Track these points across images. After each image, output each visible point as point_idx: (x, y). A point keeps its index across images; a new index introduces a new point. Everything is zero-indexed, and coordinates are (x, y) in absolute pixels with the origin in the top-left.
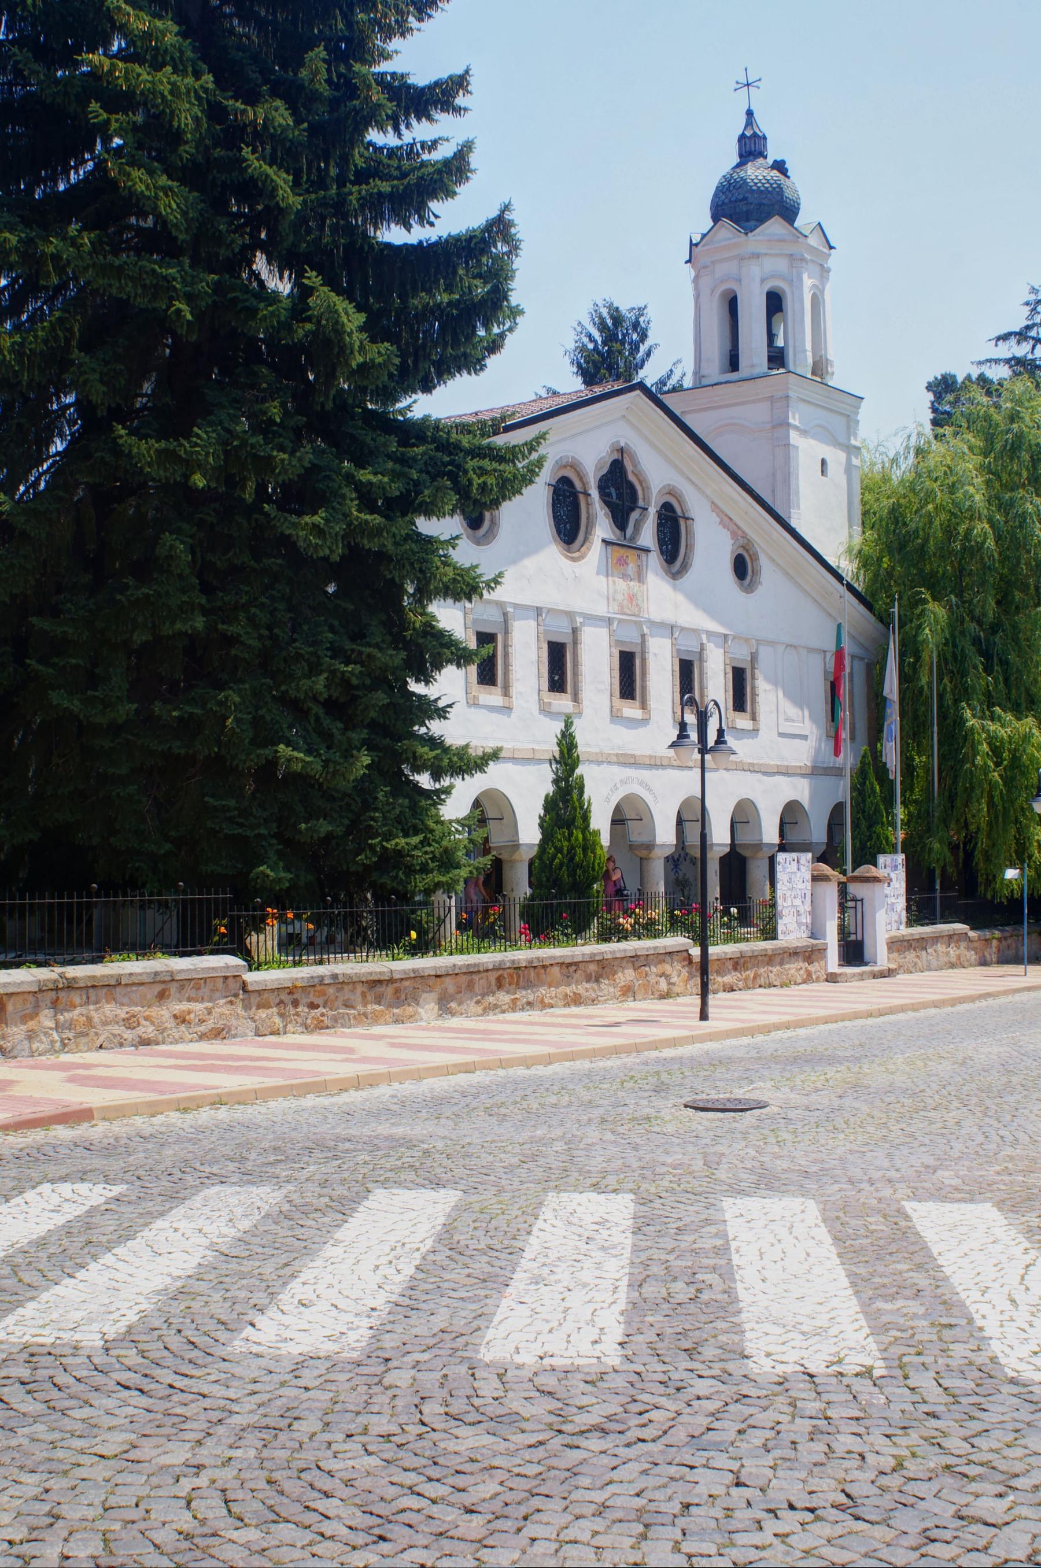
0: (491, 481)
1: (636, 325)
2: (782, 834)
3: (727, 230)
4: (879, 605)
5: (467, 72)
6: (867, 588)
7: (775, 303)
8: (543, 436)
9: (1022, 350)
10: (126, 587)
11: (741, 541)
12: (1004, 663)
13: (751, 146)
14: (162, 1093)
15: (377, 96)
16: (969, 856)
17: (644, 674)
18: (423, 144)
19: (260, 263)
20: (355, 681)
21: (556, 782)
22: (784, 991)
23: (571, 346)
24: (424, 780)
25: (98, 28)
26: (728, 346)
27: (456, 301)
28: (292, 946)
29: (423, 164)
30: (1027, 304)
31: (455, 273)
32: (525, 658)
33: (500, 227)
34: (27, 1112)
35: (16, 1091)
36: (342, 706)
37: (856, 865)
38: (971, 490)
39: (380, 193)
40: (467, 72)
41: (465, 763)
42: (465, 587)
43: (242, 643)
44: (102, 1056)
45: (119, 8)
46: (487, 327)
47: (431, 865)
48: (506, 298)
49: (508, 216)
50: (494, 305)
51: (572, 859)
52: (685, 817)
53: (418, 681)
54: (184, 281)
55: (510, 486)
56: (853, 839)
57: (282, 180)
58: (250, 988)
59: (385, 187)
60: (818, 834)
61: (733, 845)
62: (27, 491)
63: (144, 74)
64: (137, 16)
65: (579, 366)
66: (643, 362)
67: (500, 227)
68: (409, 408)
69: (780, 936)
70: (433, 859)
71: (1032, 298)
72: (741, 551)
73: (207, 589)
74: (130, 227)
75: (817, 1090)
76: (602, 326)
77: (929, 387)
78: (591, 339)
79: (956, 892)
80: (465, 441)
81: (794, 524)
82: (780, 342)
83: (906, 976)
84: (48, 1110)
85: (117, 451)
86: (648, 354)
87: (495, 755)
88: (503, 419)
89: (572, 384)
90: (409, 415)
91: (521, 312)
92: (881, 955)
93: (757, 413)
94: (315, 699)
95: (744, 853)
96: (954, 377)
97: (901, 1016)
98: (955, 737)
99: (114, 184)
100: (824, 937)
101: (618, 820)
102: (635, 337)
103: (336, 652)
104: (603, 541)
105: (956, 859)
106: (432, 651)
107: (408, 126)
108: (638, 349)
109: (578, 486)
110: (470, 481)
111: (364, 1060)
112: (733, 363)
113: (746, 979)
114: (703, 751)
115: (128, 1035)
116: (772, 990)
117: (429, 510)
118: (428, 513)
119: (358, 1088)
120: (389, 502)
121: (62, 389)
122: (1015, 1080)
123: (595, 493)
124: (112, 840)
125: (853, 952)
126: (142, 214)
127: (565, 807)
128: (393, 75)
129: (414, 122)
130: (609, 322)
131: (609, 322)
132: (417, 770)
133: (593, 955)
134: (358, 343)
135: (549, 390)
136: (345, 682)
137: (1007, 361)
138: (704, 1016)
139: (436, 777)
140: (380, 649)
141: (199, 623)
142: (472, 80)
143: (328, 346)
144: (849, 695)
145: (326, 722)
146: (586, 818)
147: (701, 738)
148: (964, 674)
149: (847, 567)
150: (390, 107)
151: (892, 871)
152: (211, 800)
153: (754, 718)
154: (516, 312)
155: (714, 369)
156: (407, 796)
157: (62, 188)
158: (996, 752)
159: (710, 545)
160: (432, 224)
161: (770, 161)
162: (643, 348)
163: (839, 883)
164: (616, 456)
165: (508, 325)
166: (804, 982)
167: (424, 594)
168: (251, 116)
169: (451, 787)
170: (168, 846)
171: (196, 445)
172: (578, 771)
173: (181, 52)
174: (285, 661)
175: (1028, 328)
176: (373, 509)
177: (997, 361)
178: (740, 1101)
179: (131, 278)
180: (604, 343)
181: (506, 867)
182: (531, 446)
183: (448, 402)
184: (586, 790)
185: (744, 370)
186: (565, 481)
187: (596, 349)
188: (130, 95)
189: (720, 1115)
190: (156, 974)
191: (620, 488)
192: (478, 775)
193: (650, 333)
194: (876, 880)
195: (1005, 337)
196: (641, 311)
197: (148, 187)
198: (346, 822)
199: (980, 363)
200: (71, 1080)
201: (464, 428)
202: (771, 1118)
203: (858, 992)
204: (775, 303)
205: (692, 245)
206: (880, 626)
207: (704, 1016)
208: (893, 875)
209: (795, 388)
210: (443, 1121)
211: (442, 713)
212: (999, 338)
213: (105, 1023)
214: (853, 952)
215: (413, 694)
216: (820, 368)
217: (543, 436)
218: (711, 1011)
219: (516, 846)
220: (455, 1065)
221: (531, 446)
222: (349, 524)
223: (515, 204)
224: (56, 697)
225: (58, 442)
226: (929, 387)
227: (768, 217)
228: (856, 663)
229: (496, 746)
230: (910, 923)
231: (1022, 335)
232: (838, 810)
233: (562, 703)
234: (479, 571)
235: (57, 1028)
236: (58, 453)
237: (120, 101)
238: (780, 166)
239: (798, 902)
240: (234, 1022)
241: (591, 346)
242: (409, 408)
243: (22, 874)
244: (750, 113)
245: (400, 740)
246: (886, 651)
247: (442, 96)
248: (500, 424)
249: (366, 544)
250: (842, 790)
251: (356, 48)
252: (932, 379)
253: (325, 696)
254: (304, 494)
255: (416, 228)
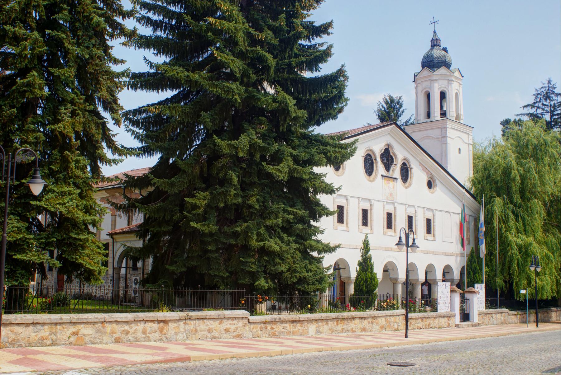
0: (338, 155)
1: (398, 102)
2: (444, 275)
3: (426, 72)
4: (479, 199)
5: (332, 21)
6: (475, 192)
7: (443, 95)
8: (357, 140)
9: (532, 111)
10: (216, 188)
11: (430, 176)
12: (523, 219)
13: (435, 43)
14: (215, 353)
15: (301, 29)
16: (511, 285)
17: (395, 220)
18: (319, 44)
19: (265, 84)
20: (291, 221)
21: (362, 256)
22: (440, 330)
23: (376, 109)
24: (315, 254)
25: (212, 10)
26: (427, 110)
27: (327, 97)
28: (272, 308)
29: (319, 51)
30: (534, 95)
31: (327, 87)
32: (353, 216)
33: (341, 72)
34: (169, 357)
35: (168, 351)
36: (287, 228)
37: (468, 287)
38: (511, 159)
39: (302, 61)
40: (332, 21)
41: (328, 249)
42: (329, 190)
43: (254, 208)
44: (200, 342)
45: (219, 3)
46: (337, 104)
47: (316, 283)
48: (343, 95)
49: (344, 69)
50: (339, 97)
51: (367, 283)
52: (428, 271)
53: (314, 221)
54: (238, 90)
55: (346, 157)
56: (467, 278)
57: (269, 56)
58: (251, 321)
59: (304, 59)
60: (456, 275)
61: (426, 279)
62: (187, 157)
63: (226, 24)
64: (224, 5)
65: (379, 116)
66: (401, 115)
67: (341, 72)
68: (313, 131)
69: (439, 311)
70: (317, 281)
71: (536, 93)
72: (430, 179)
73: (243, 189)
74: (222, 72)
75: (435, 361)
76: (387, 103)
77: (501, 123)
78: (384, 108)
79: (503, 297)
80: (331, 142)
81: (448, 170)
82: (445, 109)
83: (485, 326)
84: (176, 357)
85: (215, 144)
86: (403, 112)
87: (339, 246)
88: (344, 134)
89: (376, 122)
90: (313, 133)
91: (349, 100)
92: (475, 317)
93: (436, 133)
94: (278, 226)
95: (430, 282)
96: (510, 120)
97: (478, 339)
98: (505, 244)
99: (216, 58)
100: (455, 311)
101: (386, 270)
102: (398, 106)
103: (285, 211)
104: (382, 176)
105: (506, 285)
106: (317, 211)
107: (313, 39)
108: (399, 111)
109: (373, 157)
110: (331, 155)
111: (286, 346)
112: (429, 115)
113: (426, 325)
114: (407, 246)
115: (209, 335)
116: (435, 329)
117: (317, 164)
118: (317, 166)
119: (281, 355)
120: (303, 161)
121: (199, 123)
122: (505, 360)
123: (379, 159)
124: (210, 271)
125: (465, 317)
126: (226, 69)
127: (366, 264)
128: (310, 22)
129: (315, 38)
130: (389, 101)
131: (389, 101)
132: (312, 250)
133: (370, 315)
134: (293, 110)
135: (368, 124)
136: (288, 221)
137: (527, 114)
138: (406, 336)
139: (319, 253)
140: (300, 210)
141: (240, 200)
142: (333, 24)
143: (284, 110)
144: (470, 230)
145: (282, 234)
146: (372, 268)
147: (407, 243)
148: (508, 221)
149: (468, 185)
150: (306, 33)
151: (480, 289)
152: (243, 259)
153: (434, 236)
154: (346, 100)
155: (422, 117)
156: (308, 260)
157: (200, 60)
158: (520, 248)
159: (418, 176)
160: (319, 71)
161: (442, 48)
162: (401, 110)
163: (460, 294)
164: (386, 147)
165: (344, 104)
166: (447, 327)
167: (316, 192)
168: (260, 36)
169: (324, 257)
170: (228, 274)
171: (240, 142)
172: (369, 253)
173: (238, 16)
174: (268, 214)
175: (535, 103)
176: (298, 164)
177: (523, 114)
178: (406, 363)
179: (220, 88)
180: (388, 108)
181: (346, 285)
182: (353, 143)
183: (326, 129)
184: (372, 259)
185: (432, 118)
186: (368, 155)
187: (385, 110)
188: (222, 31)
189: (398, 367)
190: (219, 315)
191: (388, 158)
192: (333, 253)
193: (403, 105)
194: (474, 292)
195: (527, 106)
196: (400, 98)
197: (226, 59)
198: (287, 267)
199: (518, 115)
200: (187, 348)
201: (331, 137)
202: (415, 369)
203: (466, 332)
204: (443, 95)
205: (415, 76)
206: (478, 205)
207: (406, 336)
208: (480, 291)
209: (449, 124)
210: (306, 366)
211: (322, 232)
212: (524, 107)
213: (201, 331)
214: (465, 317)
215: (312, 226)
216: (458, 117)
217: (357, 140)
218: (409, 335)
219: (349, 278)
220: (315, 349)
221: (353, 143)
222: (290, 169)
223: (346, 65)
224: (192, 224)
225: (197, 141)
226: (501, 123)
227: (441, 66)
228: (471, 217)
229: (340, 242)
230: (486, 308)
231: (532, 106)
232: (463, 269)
233: (366, 230)
234: (333, 185)
235: (185, 332)
236: (197, 145)
237: (218, 32)
238: (445, 50)
239: (445, 299)
240: (245, 332)
241: (383, 109)
242: (313, 131)
243: (183, 283)
244: (435, 32)
245: (306, 241)
246: (479, 214)
247: (324, 29)
248: (342, 136)
249: (296, 175)
250: (464, 262)
251: (292, 15)
252: (502, 121)
253: (281, 225)
254: (276, 159)
255: (315, 72)
